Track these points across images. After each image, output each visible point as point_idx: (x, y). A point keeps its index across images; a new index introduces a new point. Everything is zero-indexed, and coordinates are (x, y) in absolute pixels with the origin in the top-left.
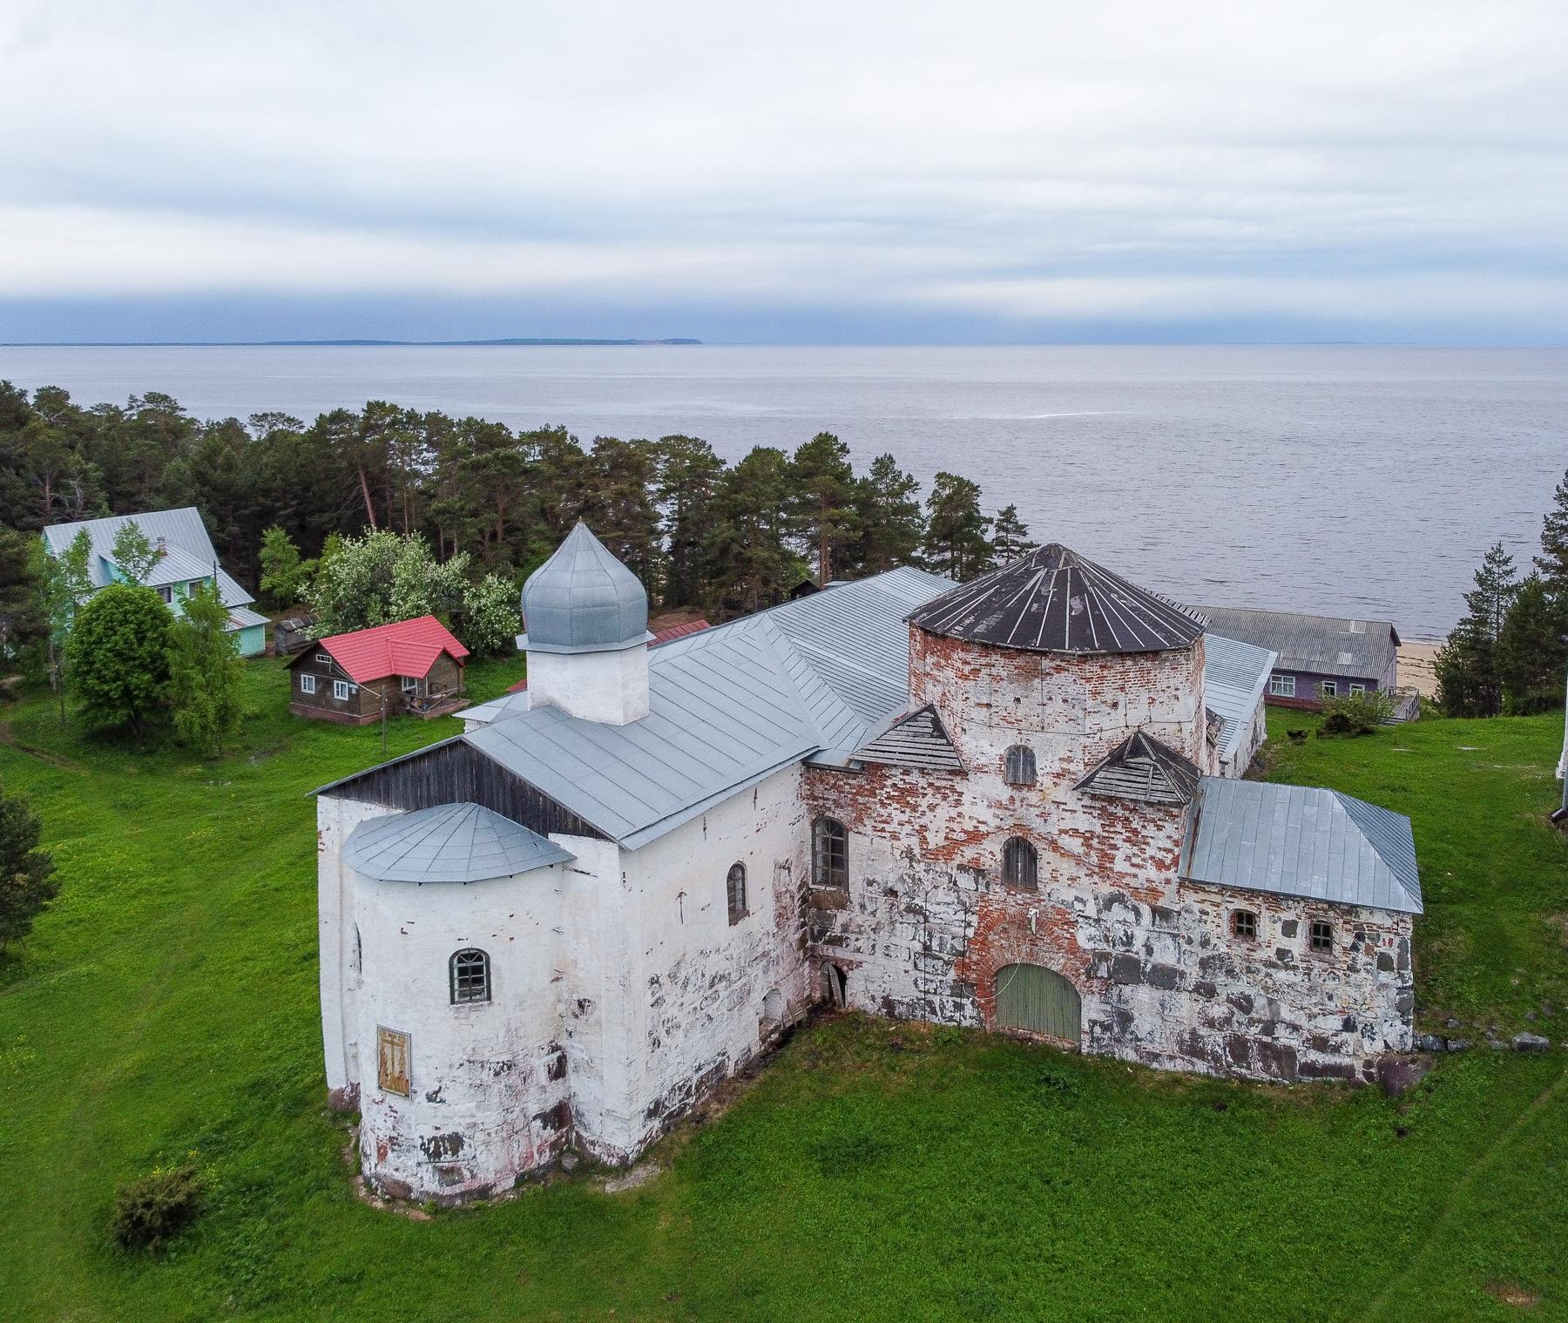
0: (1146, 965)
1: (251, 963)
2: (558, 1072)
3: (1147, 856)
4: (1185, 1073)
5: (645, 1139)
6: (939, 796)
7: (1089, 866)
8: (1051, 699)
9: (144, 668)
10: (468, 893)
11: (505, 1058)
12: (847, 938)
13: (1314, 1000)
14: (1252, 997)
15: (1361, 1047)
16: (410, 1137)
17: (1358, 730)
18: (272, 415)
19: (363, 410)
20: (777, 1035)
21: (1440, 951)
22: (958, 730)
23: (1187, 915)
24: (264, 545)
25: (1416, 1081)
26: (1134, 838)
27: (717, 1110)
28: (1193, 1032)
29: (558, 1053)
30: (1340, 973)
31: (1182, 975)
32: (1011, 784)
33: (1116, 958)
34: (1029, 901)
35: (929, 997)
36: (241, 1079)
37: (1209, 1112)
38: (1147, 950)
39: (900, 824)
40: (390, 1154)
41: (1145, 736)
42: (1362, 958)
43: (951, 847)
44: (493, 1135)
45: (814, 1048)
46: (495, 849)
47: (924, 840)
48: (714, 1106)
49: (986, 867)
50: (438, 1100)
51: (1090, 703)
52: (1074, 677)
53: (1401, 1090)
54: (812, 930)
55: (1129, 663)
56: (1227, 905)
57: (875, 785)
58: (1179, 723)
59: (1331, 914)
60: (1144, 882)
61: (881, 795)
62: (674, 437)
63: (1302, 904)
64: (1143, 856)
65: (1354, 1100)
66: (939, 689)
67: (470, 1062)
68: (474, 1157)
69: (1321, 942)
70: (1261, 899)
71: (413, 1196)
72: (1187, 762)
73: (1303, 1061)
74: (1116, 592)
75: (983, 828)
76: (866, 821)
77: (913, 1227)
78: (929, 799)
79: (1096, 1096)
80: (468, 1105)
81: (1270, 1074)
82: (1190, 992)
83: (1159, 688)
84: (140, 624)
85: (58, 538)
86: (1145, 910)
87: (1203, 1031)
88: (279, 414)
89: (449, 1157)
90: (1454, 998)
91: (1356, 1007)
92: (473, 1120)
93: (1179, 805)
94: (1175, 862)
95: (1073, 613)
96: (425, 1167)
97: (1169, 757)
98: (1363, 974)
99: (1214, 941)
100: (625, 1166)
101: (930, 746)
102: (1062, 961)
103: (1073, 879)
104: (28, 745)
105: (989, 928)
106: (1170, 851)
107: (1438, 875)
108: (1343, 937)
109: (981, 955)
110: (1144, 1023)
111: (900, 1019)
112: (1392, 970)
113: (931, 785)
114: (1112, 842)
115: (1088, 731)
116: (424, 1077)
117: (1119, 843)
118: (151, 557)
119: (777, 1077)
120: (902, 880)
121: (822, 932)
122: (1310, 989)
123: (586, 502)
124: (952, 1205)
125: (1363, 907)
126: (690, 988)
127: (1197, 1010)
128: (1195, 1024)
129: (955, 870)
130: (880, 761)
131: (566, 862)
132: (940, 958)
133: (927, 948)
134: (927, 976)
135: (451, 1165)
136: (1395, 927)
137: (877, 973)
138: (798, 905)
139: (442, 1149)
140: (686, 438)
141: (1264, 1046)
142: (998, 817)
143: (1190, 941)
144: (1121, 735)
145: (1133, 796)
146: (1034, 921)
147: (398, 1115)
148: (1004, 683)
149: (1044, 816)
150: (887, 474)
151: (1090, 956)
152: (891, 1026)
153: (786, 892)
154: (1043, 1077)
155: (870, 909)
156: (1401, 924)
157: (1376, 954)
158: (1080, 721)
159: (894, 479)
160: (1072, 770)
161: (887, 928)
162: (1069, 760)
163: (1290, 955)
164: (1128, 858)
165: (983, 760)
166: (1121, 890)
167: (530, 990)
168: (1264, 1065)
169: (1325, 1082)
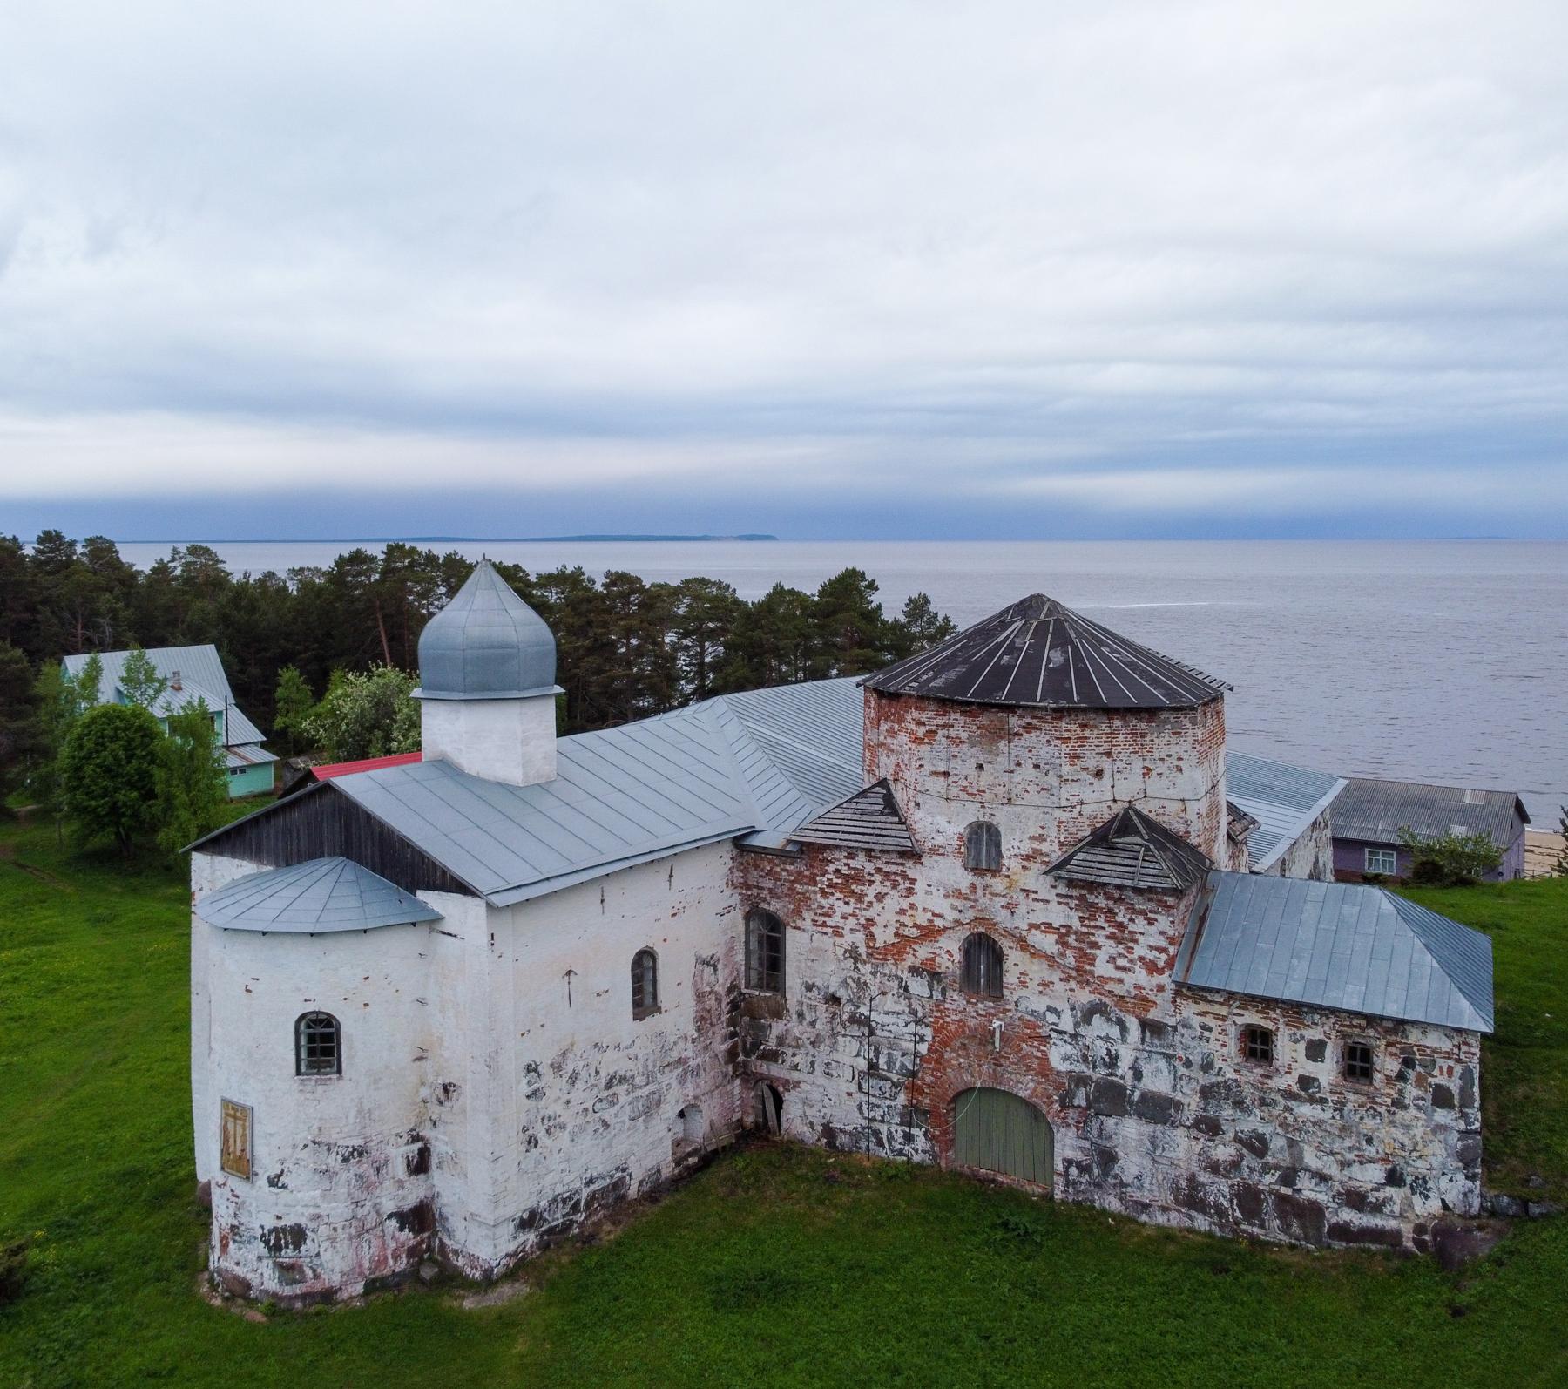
0: (1133, 1092)
1: (167, 1064)
2: (420, 1165)
3: (1135, 956)
4: (1181, 1230)
5: (515, 1254)
6: (888, 883)
7: (1064, 968)
8: (1019, 764)
9: (131, 785)
10: (318, 944)
11: (356, 1142)
12: (783, 1053)
13: (1348, 1143)
14: (1268, 1136)
15: (1411, 1206)
16: (251, 1226)
17: (1454, 879)
18: (309, 569)
19: (383, 552)
20: (696, 1159)
21: (1526, 1097)
22: (912, 804)
23: (1184, 1031)
24: (279, 685)
25: (1484, 1251)
26: (1119, 934)
27: (609, 1233)
28: (1192, 1179)
29: (420, 1145)
30: (1382, 1110)
31: (1179, 1106)
32: (972, 870)
33: (1097, 1084)
34: (992, 1011)
35: (875, 1125)
36: (114, 1168)
37: (1204, 1274)
38: (1134, 1074)
39: (844, 917)
40: (232, 1246)
41: (1138, 814)
42: (1411, 1091)
43: (901, 945)
44: (340, 1230)
45: (734, 1174)
46: (354, 902)
47: (870, 937)
48: (607, 1227)
49: (943, 969)
50: (280, 1185)
51: (1066, 769)
52: (1047, 737)
53: (1462, 1262)
54: (744, 1043)
55: (1117, 723)
56: (1236, 1018)
57: (816, 871)
58: (1183, 800)
59: (1371, 1032)
60: (1132, 989)
61: (822, 882)
62: (696, 580)
63: (1333, 1020)
64: (1130, 956)
65: (1400, 1272)
66: (893, 759)
67: (315, 1143)
68: (318, 1254)
69: (1358, 1071)
70: (1278, 1011)
71: (252, 1294)
72: (1193, 849)
73: (1334, 1220)
74: (1108, 646)
75: (939, 922)
76: (805, 914)
77: (809, 1374)
78: (877, 887)
79: (1064, 1247)
80: (312, 1193)
81: (1291, 1236)
82: (1188, 1128)
83: (1156, 755)
84: (130, 741)
85: (75, 664)
86: (1133, 1024)
87: (1205, 1177)
88: (316, 568)
89: (290, 1251)
90: (1539, 1151)
91: (1403, 1154)
92: (317, 1211)
93: (1178, 893)
94: (1170, 964)
95: (1051, 665)
96: (265, 1262)
97: (1166, 839)
98: (1413, 1111)
99: (1218, 1064)
100: (489, 1281)
101: (879, 825)
102: (1031, 1085)
103: (1045, 985)
104: (23, 863)
105: (944, 1043)
106: (1163, 950)
107: (1532, 1016)
108: (1387, 1064)
109: (935, 1077)
110: (1131, 1165)
111: (843, 1150)
112: (1452, 1107)
113: (879, 870)
114: (1092, 939)
115: (1064, 803)
116: (266, 1160)
117: (1101, 941)
118: (158, 685)
119: (685, 1202)
120: (845, 984)
121: (757, 1044)
122: (1343, 1129)
123: (596, 640)
124: (861, 1354)
125: (1413, 1023)
126: (580, 1084)
127: (1197, 1151)
128: (1195, 1169)
129: (906, 972)
130: (819, 841)
131: (433, 922)
132: (887, 1079)
133: (873, 1066)
134: (873, 1100)
135: (292, 1261)
136: (1456, 1051)
137: (816, 1095)
138: (726, 1010)
139: (283, 1241)
140: (709, 582)
141: (1282, 1199)
142: (956, 908)
143: (1188, 1064)
144: (1106, 811)
145: (1118, 882)
146: (998, 1035)
147: (239, 1201)
148: (964, 747)
149: (1011, 907)
150: (922, 617)
151: (1065, 1080)
152: (830, 1157)
153: (710, 993)
154: (999, 1221)
155: (809, 1019)
156: (1465, 1048)
157: (1430, 1085)
158: (1054, 791)
159: (930, 624)
160: (1044, 850)
161: (827, 1042)
162: (1041, 838)
163: (1316, 1084)
164: (1112, 959)
165: (939, 840)
166: (1103, 999)
167: (387, 1067)
168: (1282, 1222)
169: (1363, 1250)
